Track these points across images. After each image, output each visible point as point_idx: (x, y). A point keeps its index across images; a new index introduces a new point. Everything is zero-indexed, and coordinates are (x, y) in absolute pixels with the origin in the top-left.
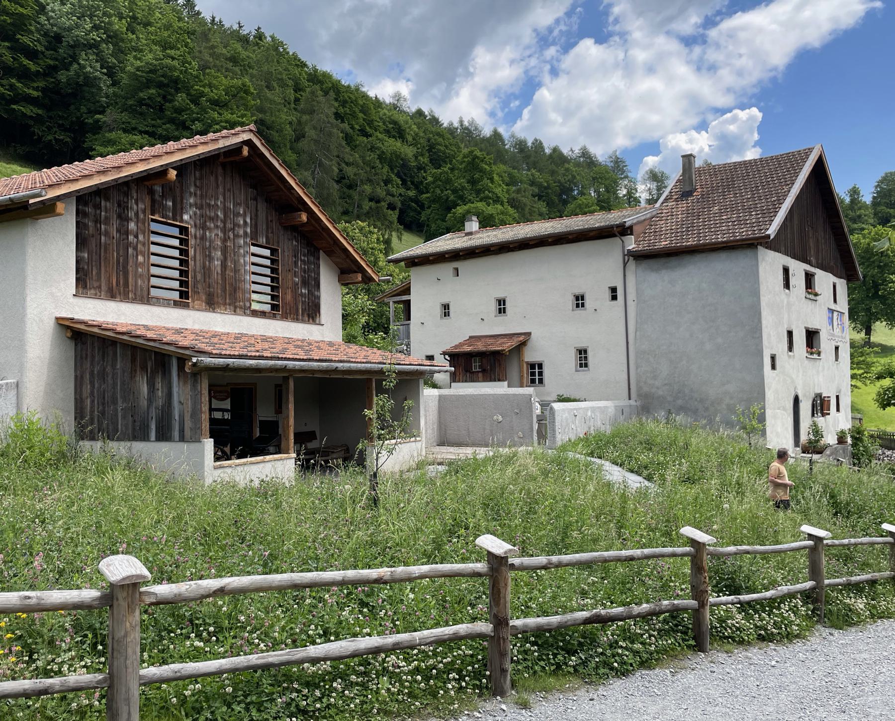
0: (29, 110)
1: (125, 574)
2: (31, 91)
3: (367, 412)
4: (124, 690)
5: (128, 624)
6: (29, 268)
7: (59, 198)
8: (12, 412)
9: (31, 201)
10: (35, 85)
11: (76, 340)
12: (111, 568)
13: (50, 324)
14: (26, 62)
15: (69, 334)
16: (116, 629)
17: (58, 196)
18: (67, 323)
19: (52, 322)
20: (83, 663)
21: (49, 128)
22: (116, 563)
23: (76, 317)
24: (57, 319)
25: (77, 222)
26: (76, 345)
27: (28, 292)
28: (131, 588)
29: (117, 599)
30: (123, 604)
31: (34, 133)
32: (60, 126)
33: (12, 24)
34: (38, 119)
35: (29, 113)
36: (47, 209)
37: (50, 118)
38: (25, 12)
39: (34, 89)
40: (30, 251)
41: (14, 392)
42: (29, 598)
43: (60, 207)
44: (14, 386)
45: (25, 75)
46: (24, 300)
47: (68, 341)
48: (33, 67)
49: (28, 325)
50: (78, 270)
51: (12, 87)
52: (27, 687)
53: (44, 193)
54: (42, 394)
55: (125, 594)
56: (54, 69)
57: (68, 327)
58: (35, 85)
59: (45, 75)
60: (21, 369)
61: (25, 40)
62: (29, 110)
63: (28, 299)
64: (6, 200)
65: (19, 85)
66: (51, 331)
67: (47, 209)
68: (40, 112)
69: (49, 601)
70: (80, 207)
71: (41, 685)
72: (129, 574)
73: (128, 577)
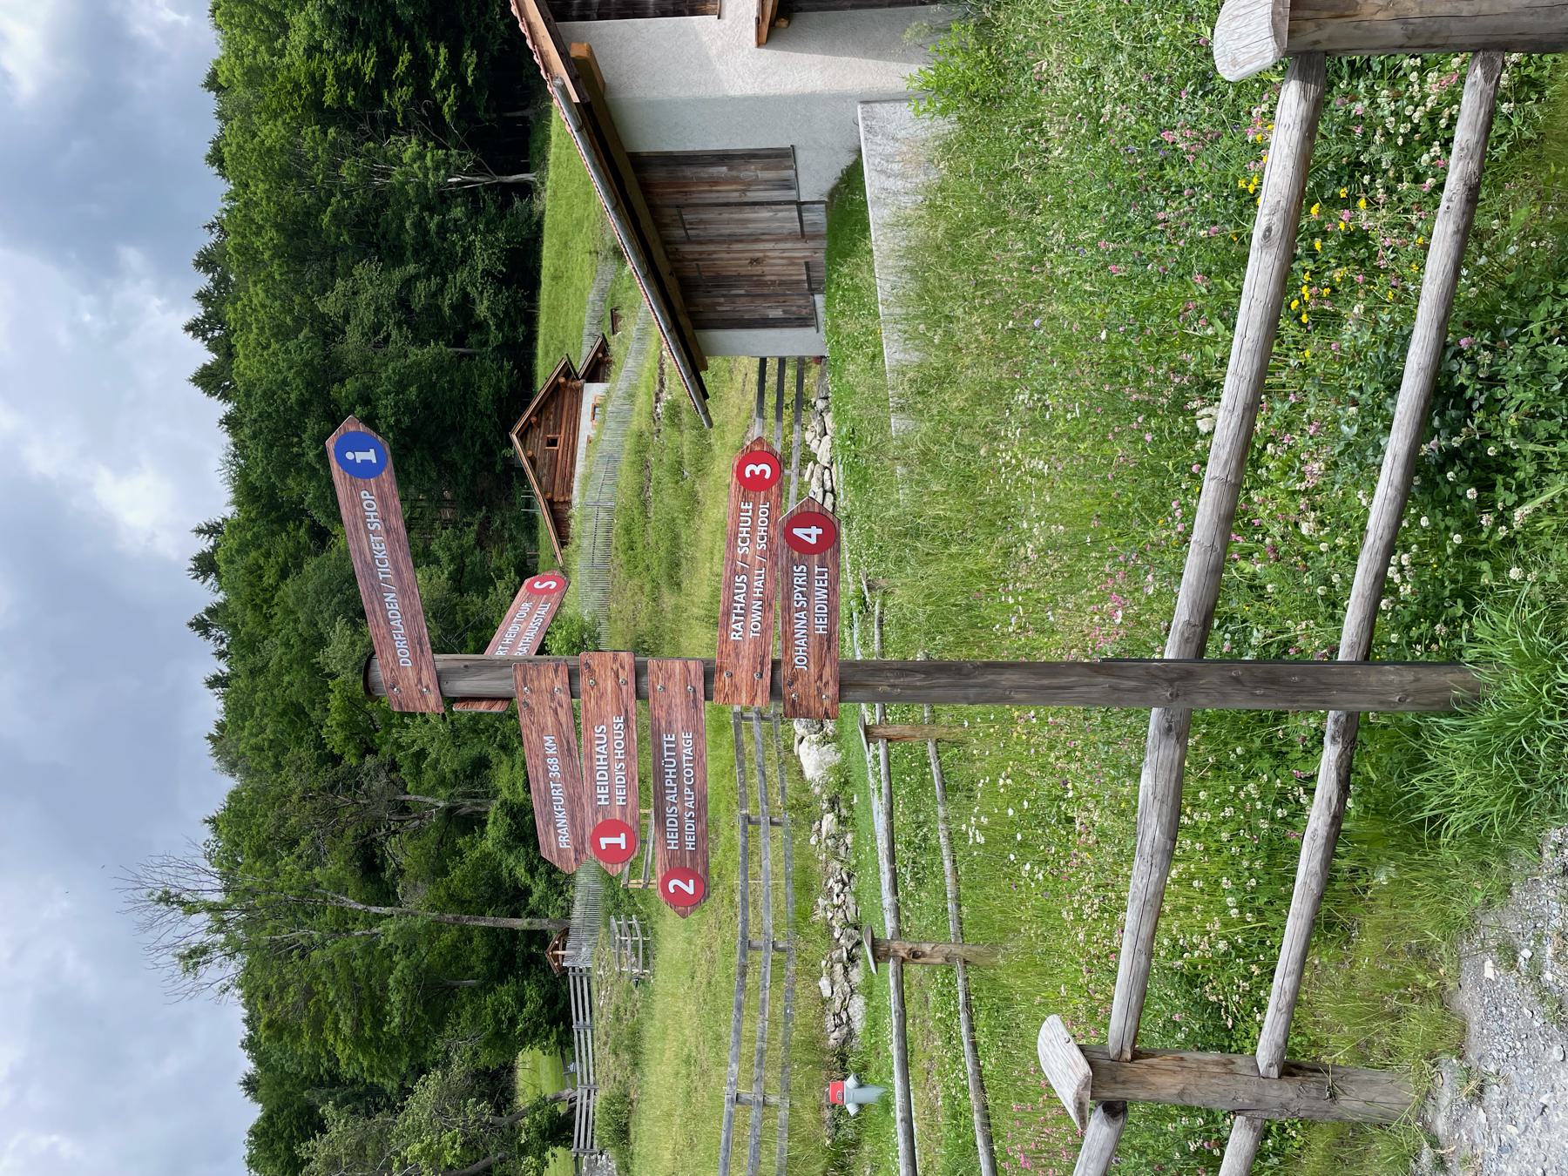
0: (470, 59)
1: (1265, 30)
2: (441, 58)
3: (820, 531)
4: (1525, 19)
5: (1379, 16)
6: (682, 94)
7: (564, 54)
8: (905, 110)
9: (576, 99)
10: (431, 51)
11: (792, 11)
12: (1241, 58)
13: (769, 55)
14: (401, 68)
15: (784, 23)
16: (1384, 42)
17: (561, 54)
18: (765, 29)
19: (766, 52)
20: (1414, 76)
21: (488, 28)
22: (1232, 45)
23: (754, 13)
24: (759, 45)
25: (600, 17)
26: (801, 10)
27: (720, 94)
28: (1299, 14)
29: (1317, 42)
30: (1333, 27)
31: (501, 51)
32: (482, 13)
33: (355, 89)
34: (479, 46)
35: (474, 59)
36: (584, 71)
37: (473, 27)
38: (330, 73)
39: (437, 54)
40: (655, 93)
41: (877, 107)
42: (1269, 229)
43: (577, 51)
44: (867, 107)
45: (421, 67)
46: (733, 99)
47: (795, 23)
48: (405, 58)
49: (771, 91)
50: (678, 13)
51: (443, 85)
52: (1451, 228)
53: (558, 82)
54: (881, 63)
55: (1310, 26)
56: (398, 25)
57: (772, 25)
58: (431, 51)
59: (410, 37)
60: (842, 97)
61: (368, 70)
62: (470, 59)
63: (732, 93)
64: (582, 137)
65: (437, 75)
66: (778, 52)
67: (584, 71)
68: (468, 44)
69: (1285, 191)
70: (574, 13)
71: (1456, 199)
72: (1267, 22)
73: (1274, 24)
